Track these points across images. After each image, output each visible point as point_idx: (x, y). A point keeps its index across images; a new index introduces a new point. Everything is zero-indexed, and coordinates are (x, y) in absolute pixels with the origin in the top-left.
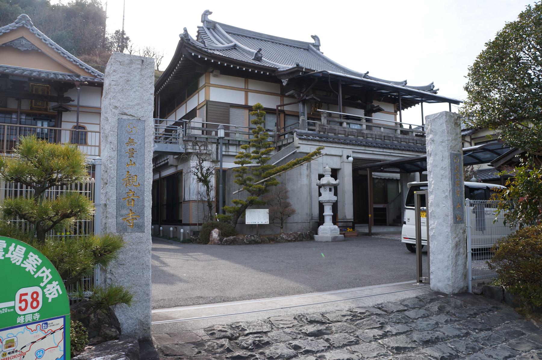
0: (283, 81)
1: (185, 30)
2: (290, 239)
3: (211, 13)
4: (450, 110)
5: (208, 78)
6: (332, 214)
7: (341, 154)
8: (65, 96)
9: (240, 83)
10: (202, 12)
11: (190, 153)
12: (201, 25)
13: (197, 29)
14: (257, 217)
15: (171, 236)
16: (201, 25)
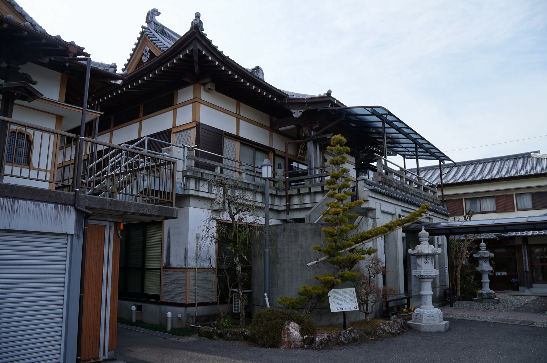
0: (293, 111)
1: (198, 16)
2: (394, 331)
3: (159, 14)
4: (405, 167)
5: (196, 92)
6: (432, 293)
7: (393, 212)
8: (20, 71)
9: (230, 105)
10: (150, 9)
11: (189, 196)
12: (146, 25)
13: (141, 30)
14: (343, 301)
15: (134, 320)
16: (146, 25)
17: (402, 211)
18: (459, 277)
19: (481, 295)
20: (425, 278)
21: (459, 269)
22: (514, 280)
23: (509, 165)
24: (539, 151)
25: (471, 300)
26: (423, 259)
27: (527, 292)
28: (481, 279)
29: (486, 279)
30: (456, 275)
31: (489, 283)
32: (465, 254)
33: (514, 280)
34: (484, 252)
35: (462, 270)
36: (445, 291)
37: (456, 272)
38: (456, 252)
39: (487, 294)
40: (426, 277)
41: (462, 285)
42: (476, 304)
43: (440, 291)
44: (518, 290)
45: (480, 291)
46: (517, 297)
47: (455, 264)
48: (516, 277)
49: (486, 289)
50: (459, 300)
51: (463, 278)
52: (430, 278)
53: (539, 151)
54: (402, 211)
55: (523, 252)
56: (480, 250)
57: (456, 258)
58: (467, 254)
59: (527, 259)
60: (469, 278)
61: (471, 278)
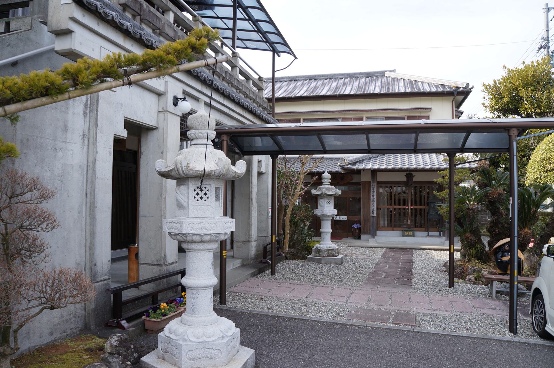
17: (185, 92)
18: (288, 223)
19: (319, 251)
20: (193, 242)
21: (289, 211)
22: (355, 226)
23: (359, 82)
24: (395, 70)
25: (304, 258)
26: (192, 185)
27: (372, 242)
28: (320, 228)
29: (327, 228)
30: (284, 219)
31: (332, 233)
32: (299, 189)
33: (355, 226)
34: (327, 187)
35: (293, 213)
36: (265, 248)
37: (285, 215)
38: (287, 187)
39: (328, 250)
40: (196, 238)
41: (292, 235)
42: (311, 266)
43: (258, 246)
44: (359, 238)
45: (317, 246)
46: (361, 250)
47: (283, 203)
48: (359, 222)
49: (326, 243)
50: (286, 258)
51: (294, 224)
52: (210, 241)
53: (395, 70)
54: (185, 92)
55: (372, 190)
56: (321, 184)
57: (286, 195)
58: (302, 189)
59: (375, 200)
60: (302, 225)
61: (305, 225)
